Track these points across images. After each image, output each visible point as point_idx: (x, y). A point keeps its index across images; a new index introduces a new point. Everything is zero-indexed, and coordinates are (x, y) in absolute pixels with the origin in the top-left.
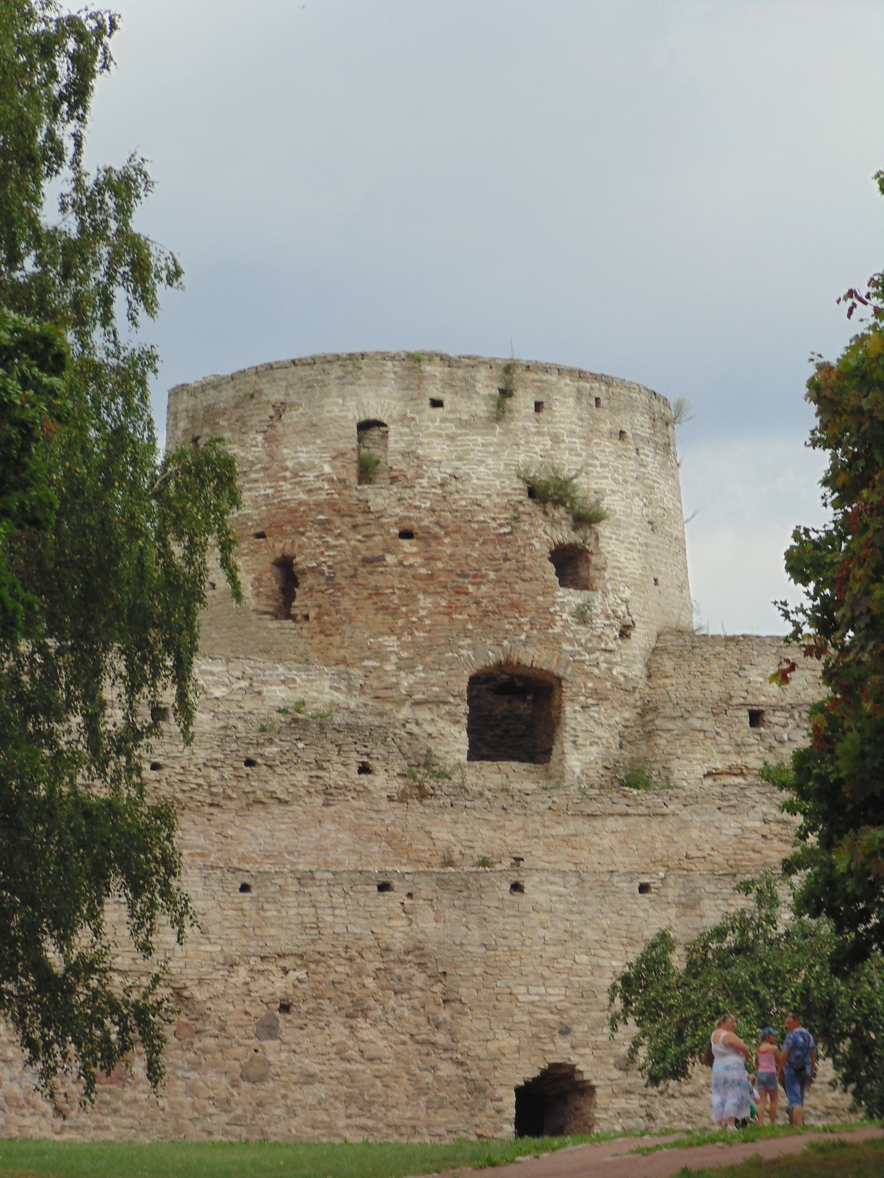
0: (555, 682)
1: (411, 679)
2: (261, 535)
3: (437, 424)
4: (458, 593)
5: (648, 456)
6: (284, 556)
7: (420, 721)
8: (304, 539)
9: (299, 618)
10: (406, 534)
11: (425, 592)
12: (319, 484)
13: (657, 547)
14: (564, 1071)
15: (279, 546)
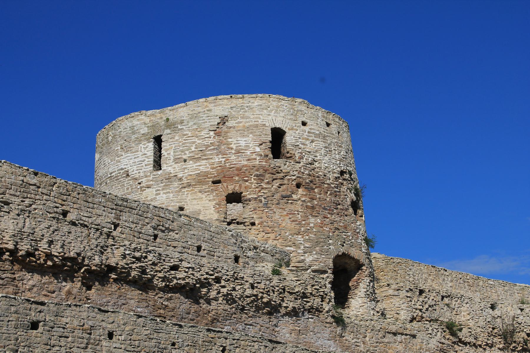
3: (307, 133)
4: (325, 218)
8: (247, 183)
10: (298, 186)
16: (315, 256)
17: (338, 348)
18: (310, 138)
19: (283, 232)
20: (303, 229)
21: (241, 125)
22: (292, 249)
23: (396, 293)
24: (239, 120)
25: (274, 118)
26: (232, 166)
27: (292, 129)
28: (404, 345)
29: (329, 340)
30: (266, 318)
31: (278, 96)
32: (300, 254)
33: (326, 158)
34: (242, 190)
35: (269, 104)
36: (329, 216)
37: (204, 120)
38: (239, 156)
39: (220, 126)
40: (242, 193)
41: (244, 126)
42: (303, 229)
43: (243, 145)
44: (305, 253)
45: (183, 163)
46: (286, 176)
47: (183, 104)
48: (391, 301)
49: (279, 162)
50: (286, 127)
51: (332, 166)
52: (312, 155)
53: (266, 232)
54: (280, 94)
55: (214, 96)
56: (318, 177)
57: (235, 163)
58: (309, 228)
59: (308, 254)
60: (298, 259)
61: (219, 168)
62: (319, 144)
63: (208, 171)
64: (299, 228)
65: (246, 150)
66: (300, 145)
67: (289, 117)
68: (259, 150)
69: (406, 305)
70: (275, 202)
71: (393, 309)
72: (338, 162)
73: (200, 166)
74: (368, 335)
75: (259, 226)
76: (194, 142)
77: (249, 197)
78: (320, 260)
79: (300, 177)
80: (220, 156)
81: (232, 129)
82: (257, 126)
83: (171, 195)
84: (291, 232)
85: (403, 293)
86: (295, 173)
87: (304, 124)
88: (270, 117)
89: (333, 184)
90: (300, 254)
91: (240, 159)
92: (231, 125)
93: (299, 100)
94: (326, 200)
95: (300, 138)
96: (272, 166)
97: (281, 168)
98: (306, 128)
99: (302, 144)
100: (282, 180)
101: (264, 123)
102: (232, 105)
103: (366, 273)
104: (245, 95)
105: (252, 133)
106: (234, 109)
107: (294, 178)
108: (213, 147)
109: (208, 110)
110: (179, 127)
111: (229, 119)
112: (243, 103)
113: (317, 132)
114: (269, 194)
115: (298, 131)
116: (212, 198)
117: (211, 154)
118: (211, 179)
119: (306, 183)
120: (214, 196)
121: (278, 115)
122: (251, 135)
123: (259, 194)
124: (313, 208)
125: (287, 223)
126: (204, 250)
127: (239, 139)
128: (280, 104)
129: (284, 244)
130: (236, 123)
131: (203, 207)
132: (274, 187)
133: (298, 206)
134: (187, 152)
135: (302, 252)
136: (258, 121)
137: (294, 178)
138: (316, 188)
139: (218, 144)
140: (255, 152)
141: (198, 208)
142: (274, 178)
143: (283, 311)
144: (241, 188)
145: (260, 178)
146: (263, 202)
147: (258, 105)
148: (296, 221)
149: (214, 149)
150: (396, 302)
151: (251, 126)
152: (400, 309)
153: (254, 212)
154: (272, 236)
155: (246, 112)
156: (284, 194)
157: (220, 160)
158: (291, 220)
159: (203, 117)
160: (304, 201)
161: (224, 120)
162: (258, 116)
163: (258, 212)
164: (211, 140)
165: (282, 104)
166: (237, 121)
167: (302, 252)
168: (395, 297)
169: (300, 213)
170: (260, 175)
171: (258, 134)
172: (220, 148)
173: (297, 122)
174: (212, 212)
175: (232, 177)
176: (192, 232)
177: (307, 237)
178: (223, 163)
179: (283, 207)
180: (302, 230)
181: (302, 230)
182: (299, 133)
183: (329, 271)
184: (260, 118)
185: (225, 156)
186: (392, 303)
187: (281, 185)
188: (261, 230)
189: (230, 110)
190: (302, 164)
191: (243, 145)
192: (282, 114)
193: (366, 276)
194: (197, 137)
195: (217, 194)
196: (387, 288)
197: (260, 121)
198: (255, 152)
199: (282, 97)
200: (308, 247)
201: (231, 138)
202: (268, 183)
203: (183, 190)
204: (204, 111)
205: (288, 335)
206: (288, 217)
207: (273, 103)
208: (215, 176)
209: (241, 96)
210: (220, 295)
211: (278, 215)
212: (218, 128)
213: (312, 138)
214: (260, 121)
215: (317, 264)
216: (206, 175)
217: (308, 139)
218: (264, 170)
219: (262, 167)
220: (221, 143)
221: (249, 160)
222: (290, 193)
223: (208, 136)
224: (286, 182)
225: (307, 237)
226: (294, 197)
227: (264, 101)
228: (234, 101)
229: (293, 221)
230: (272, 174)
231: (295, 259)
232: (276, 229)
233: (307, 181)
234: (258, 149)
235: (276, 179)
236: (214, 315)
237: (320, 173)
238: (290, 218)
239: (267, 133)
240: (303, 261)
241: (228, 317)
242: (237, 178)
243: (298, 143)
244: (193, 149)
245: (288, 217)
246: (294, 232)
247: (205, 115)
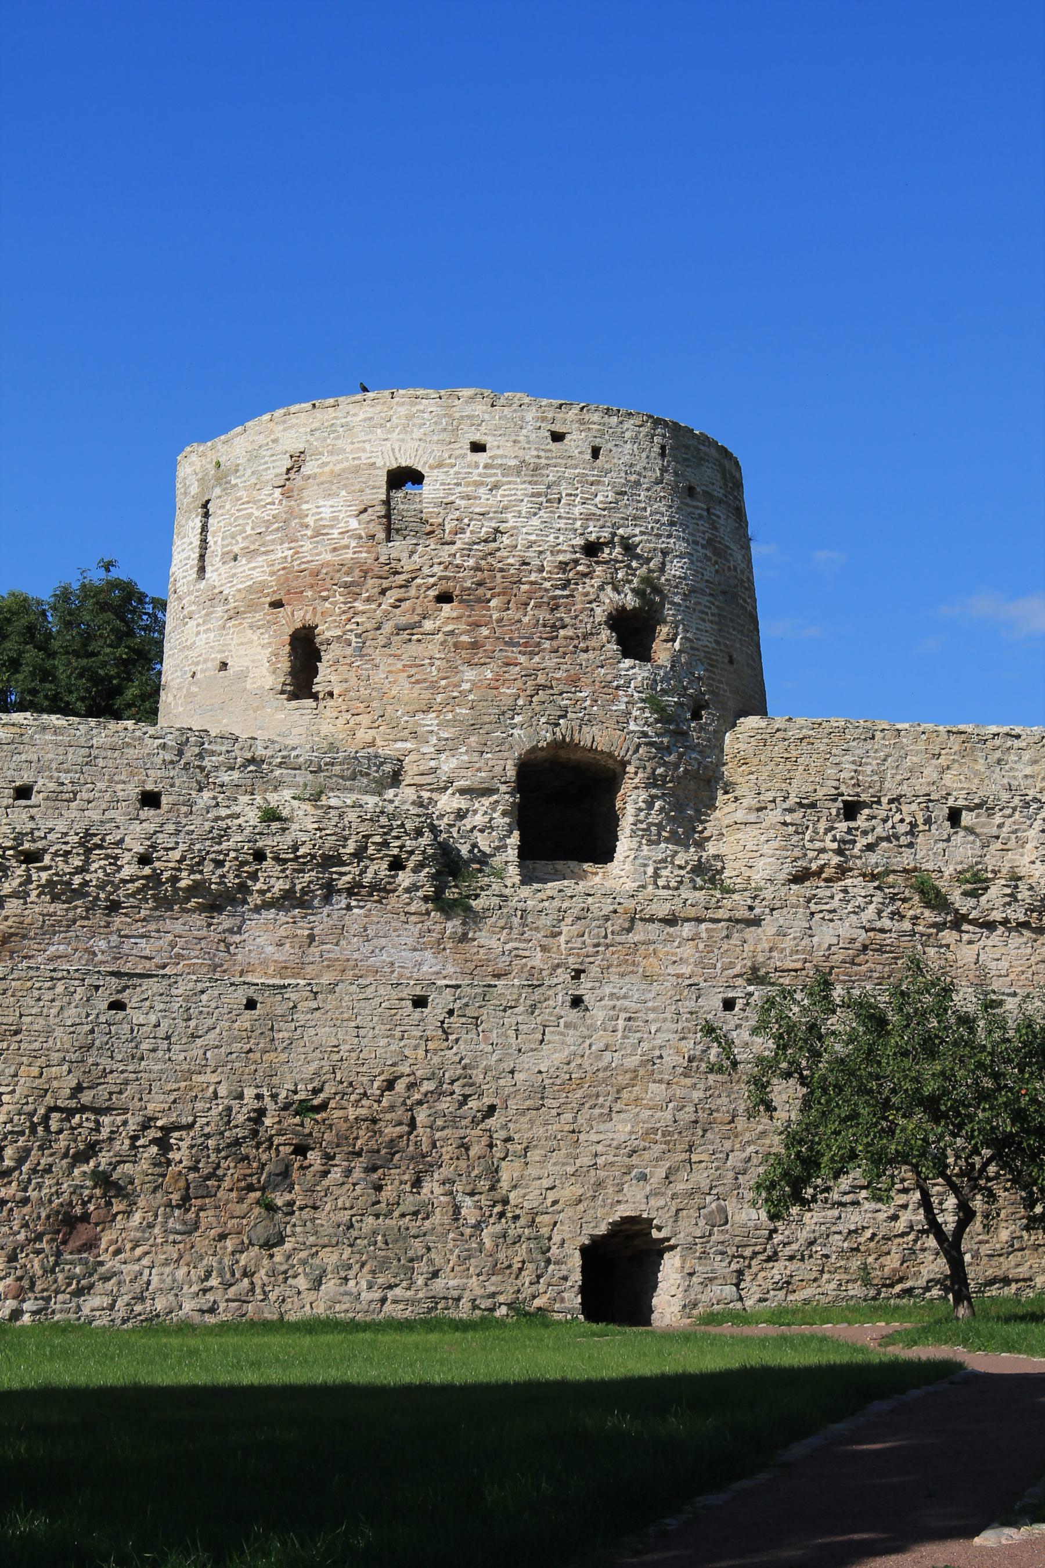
0: (619, 769)
1: (454, 763)
2: (277, 604)
3: (481, 470)
4: (508, 664)
5: (719, 517)
6: (304, 627)
7: (692, 1271)
8: (327, 605)
9: (321, 696)
10: (444, 598)
11: (470, 664)
12: (345, 542)
13: (732, 620)
14: (637, 1227)
15: (299, 615)
16: (465, 758)
17: (449, 966)
18: (489, 480)
19: (389, 708)
20: (439, 698)
21: (327, 469)
22: (408, 745)
23: (752, 817)
24: (324, 459)
25: (396, 446)
26: (303, 566)
27: (440, 466)
28: (701, 946)
29: (415, 950)
30: (198, 920)
31: (412, 392)
32: (428, 756)
33: (535, 521)
34: (317, 621)
35: (391, 413)
36: (522, 659)
37: (266, 463)
38: (317, 542)
39: (292, 475)
40: (317, 626)
41: (332, 472)
42: (439, 698)
43: (327, 516)
44: (439, 752)
45: (232, 563)
46: (413, 579)
47: (239, 429)
48: (737, 837)
49: (399, 547)
50: (425, 463)
51: (551, 538)
52: (491, 519)
53: (355, 711)
54: (415, 386)
55: (333, 397)
56: (501, 570)
57: (309, 558)
58: (455, 694)
59: (447, 753)
60: (421, 768)
61: (282, 572)
62: (518, 489)
63: (264, 581)
64: (430, 696)
65: (332, 527)
66: (458, 502)
67: (435, 438)
68: (357, 526)
69: (775, 844)
70: (382, 640)
71: (739, 855)
72: (579, 523)
73: (254, 568)
74: (565, 929)
75: (340, 700)
76: (251, 515)
77: (328, 634)
78: (477, 765)
79: (448, 578)
80: (286, 545)
81: (311, 480)
82: (356, 470)
83: (212, 635)
84: (408, 709)
85: (774, 816)
86: (436, 569)
87: (478, 447)
88: (388, 444)
89: (549, 579)
90: (428, 756)
91: (320, 549)
92: (309, 472)
93: (466, 392)
94: (520, 621)
95: (458, 484)
96: (382, 559)
97: (402, 563)
98: (482, 458)
99: (463, 498)
100: (403, 590)
101: (372, 460)
102: (314, 426)
103: (637, 780)
104: (341, 399)
105: (345, 486)
106: (317, 434)
107: (432, 580)
108: (276, 525)
109: (273, 441)
110: (233, 482)
111: (308, 458)
112: (335, 418)
113: (513, 463)
114: (369, 626)
115: (456, 469)
116: (266, 641)
117: (273, 540)
118: (268, 599)
119: (464, 589)
120: (270, 636)
121: (408, 437)
122: (343, 493)
123: (348, 627)
124: (475, 645)
125: (402, 688)
126: (39, 792)
127: (322, 503)
128: (414, 409)
129: (391, 737)
130: (319, 467)
131: (253, 661)
132: (383, 607)
133: (433, 648)
134: (239, 538)
135: (432, 750)
136: (359, 458)
137: (432, 580)
138: (493, 596)
139: (284, 516)
140: (347, 532)
141: (245, 664)
142: (384, 586)
143: (255, 899)
144: (315, 616)
145: (352, 589)
146: (354, 644)
147: (365, 420)
148: (425, 680)
149: (277, 530)
150: (749, 837)
151: (344, 470)
152: (758, 854)
153: (333, 668)
154: (365, 719)
155: (337, 438)
156: (403, 621)
157: (284, 555)
158: (413, 680)
159: (264, 456)
160: (452, 633)
161: (297, 462)
162: (361, 445)
163: (341, 668)
164: (274, 509)
165: (422, 408)
166: (320, 462)
167: (432, 750)
168: (749, 828)
169: (438, 663)
170: (352, 584)
171: (358, 487)
172: (288, 526)
173: (456, 446)
174: (265, 672)
175: (302, 592)
176: (24, 757)
177: (450, 716)
178: (289, 560)
179: (399, 652)
180: (439, 700)
181: (439, 700)
182: (456, 473)
183: (503, 788)
184: (364, 450)
185: (292, 545)
186: (738, 841)
187: (400, 600)
188: (344, 708)
189: (309, 437)
190: (459, 545)
191: (327, 516)
192: (418, 433)
193: (636, 788)
194: (255, 502)
195: (275, 631)
196: (735, 805)
197: (363, 456)
198: (347, 532)
199: (421, 392)
200: (447, 739)
201: (307, 502)
202: (368, 600)
203: (230, 624)
204: (268, 444)
205: (270, 949)
206: (406, 674)
207: (400, 409)
208: (274, 592)
209: (331, 401)
210: (31, 887)
211: (383, 671)
212: (288, 479)
213: (493, 479)
214: (363, 456)
215: (470, 774)
216: (258, 589)
217: (482, 484)
218: (361, 570)
219: (357, 563)
220: (290, 511)
221: (335, 550)
222: (417, 618)
223: (270, 500)
224: (413, 592)
225: (450, 716)
226: (428, 625)
227: (379, 408)
228: (318, 414)
229: (417, 682)
230: (381, 578)
231: (415, 768)
232: (374, 704)
233: (468, 584)
234: (354, 524)
235: (390, 588)
236: (11, 927)
237: (511, 561)
238: (409, 677)
239: (377, 484)
240: (434, 771)
241: (49, 929)
242: (310, 593)
243: (452, 498)
244: (249, 531)
245: (406, 674)
246: (416, 707)
247: (269, 453)
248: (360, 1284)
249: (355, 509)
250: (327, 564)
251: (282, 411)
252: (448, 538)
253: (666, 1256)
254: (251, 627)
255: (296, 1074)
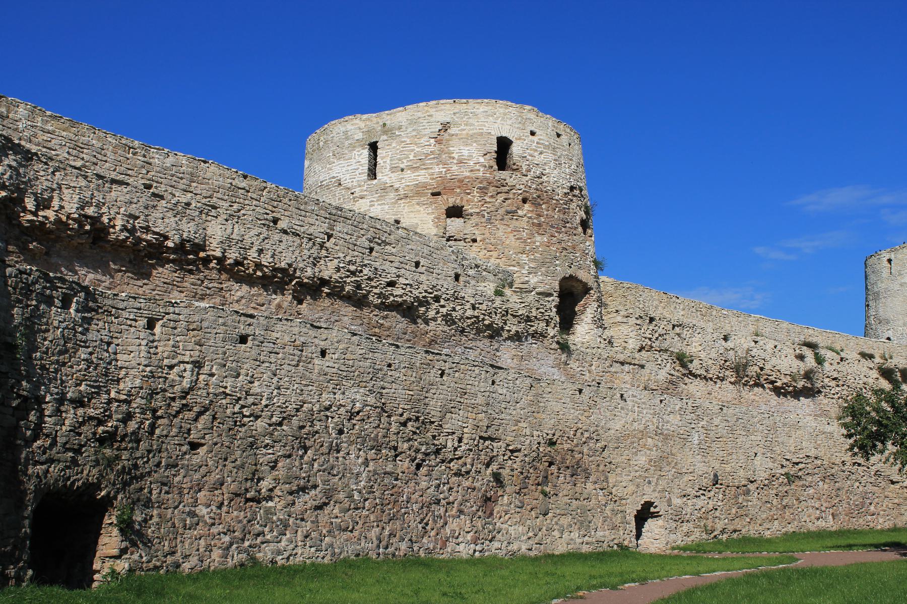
1: (536, 279)
10: (525, 201)
12: (477, 167)
20: (528, 248)
22: (516, 269)
23: (625, 320)
27: (520, 139)
30: (487, 341)
39: (442, 133)
42: (528, 248)
44: (529, 273)
47: (401, 108)
49: (504, 174)
54: (507, 100)
69: (634, 333)
70: (499, 217)
82: (481, 134)
83: (387, 207)
85: (632, 321)
86: (522, 187)
87: (533, 133)
93: (528, 107)
98: (535, 138)
106: (457, 115)
114: (492, 209)
125: (511, 241)
133: (524, 223)
134: (405, 161)
143: (505, 335)
145: (483, 190)
150: (624, 329)
154: (495, 254)
160: (530, 218)
161: (445, 127)
164: (432, 148)
170: (484, 188)
174: (431, 227)
176: (410, 247)
183: (555, 294)
190: (529, 177)
192: (509, 122)
199: (509, 103)
202: (492, 197)
209: (465, 101)
216: (425, 186)
220: (442, 151)
221: (472, 171)
224: (511, 196)
226: (520, 213)
228: (457, 106)
229: (518, 239)
232: (499, 247)
234: (482, 160)
240: (527, 282)
242: (458, 190)
248: (575, 535)
249: (482, 153)
250: (468, 177)
251: (434, 102)
252: (525, 173)
253: (649, 520)
254: (418, 204)
255: (549, 425)
